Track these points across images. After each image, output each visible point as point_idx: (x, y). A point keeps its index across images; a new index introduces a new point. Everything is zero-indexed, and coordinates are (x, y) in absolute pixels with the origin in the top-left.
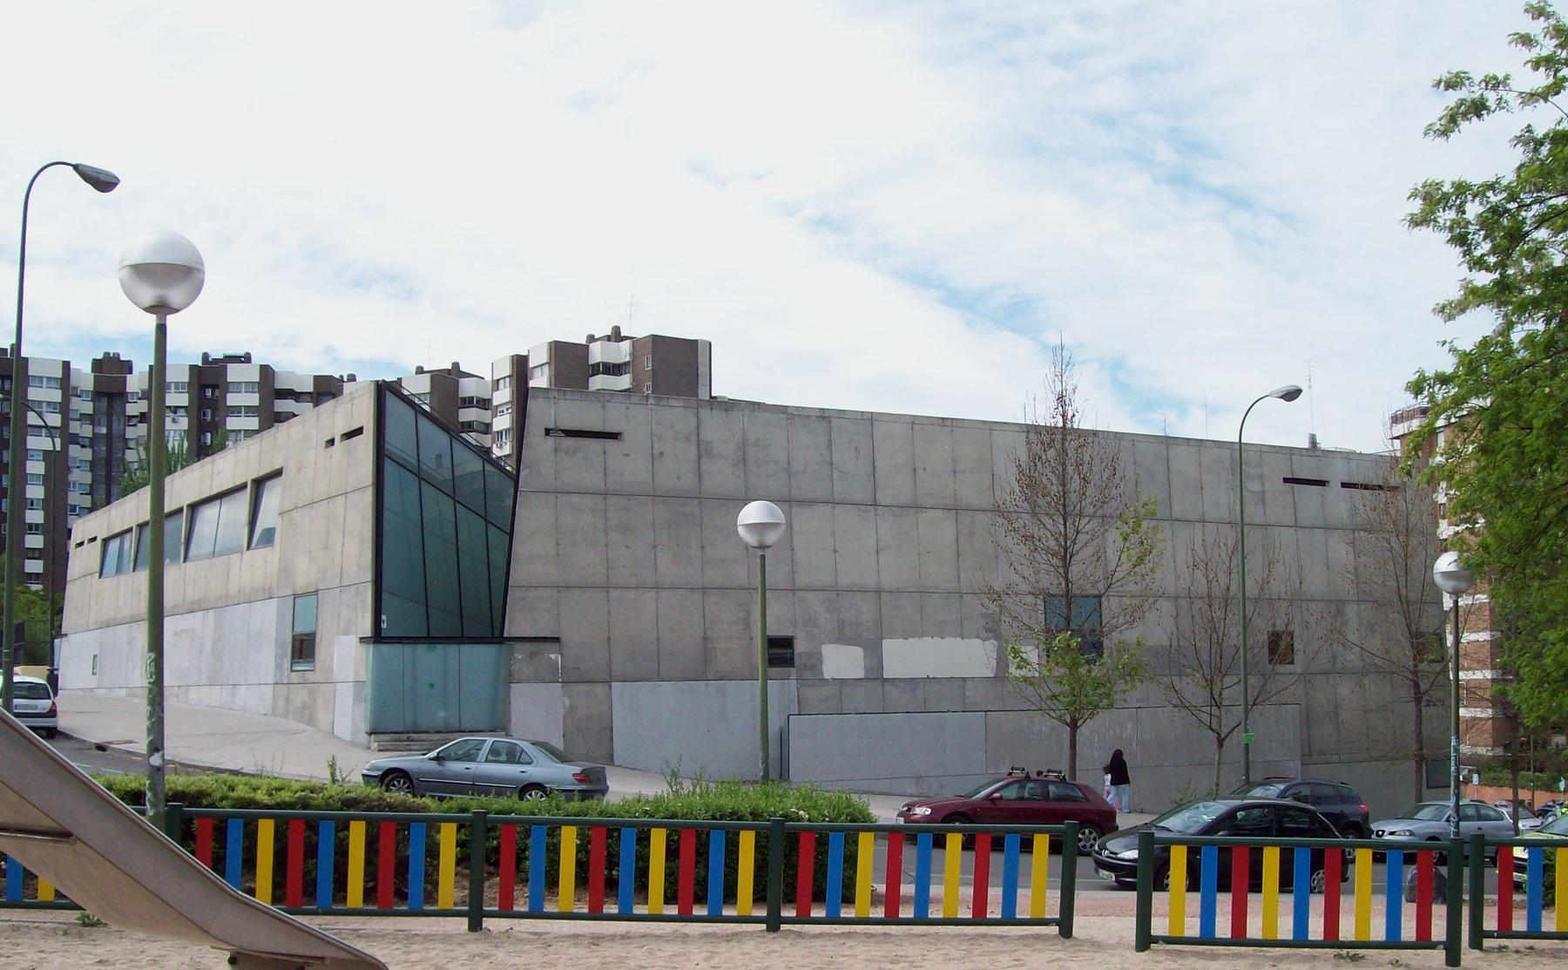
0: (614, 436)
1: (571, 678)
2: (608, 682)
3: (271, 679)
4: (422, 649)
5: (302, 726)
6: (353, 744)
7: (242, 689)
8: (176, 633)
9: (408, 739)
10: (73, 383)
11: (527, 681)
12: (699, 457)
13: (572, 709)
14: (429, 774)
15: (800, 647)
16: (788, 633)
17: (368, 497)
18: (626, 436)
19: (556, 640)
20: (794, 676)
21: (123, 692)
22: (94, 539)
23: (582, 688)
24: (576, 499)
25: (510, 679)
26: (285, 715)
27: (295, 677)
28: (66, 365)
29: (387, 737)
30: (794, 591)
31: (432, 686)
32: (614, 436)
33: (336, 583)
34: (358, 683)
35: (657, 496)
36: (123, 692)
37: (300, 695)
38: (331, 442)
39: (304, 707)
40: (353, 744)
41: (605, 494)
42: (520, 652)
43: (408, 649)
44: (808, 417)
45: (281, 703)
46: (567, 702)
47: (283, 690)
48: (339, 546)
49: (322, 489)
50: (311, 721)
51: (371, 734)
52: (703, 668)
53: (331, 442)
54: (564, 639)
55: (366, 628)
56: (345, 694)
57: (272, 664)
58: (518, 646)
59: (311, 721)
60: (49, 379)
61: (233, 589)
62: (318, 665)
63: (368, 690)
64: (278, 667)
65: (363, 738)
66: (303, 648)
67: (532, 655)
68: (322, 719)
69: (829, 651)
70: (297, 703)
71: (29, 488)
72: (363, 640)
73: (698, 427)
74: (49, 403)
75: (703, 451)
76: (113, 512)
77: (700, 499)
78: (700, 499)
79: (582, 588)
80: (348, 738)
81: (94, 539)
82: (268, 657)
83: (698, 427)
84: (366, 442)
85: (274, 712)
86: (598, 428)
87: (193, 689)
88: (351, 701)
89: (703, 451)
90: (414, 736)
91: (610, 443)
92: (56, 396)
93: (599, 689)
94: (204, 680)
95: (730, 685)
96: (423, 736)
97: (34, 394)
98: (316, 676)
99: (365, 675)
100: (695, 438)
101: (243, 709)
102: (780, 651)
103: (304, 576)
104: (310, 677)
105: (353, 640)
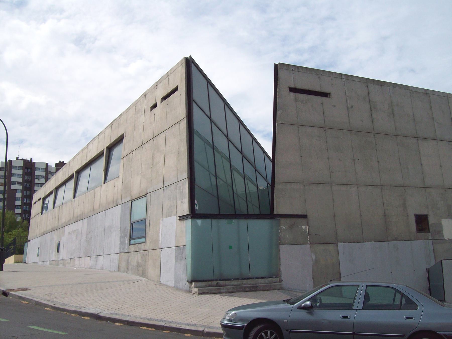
0: (326, 95)
1: (315, 241)
2: (336, 243)
3: (117, 250)
4: (223, 222)
5: (139, 278)
6: (177, 288)
7: (101, 258)
8: (69, 233)
9: (218, 285)
10: (49, 170)
11: (289, 244)
12: (371, 110)
13: (317, 261)
14: (300, 323)
15: (431, 220)
16: (425, 212)
17: (184, 125)
18: (333, 95)
19: (304, 216)
20: (430, 238)
21: (48, 263)
22: (40, 199)
23: (321, 247)
24: (309, 130)
25: (279, 242)
26: (127, 270)
27: (132, 248)
28: (47, 164)
29: (203, 284)
30: (425, 188)
31: (231, 247)
32: (326, 95)
33: (161, 185)
34: (180, 248)
35: (353, 131)
36: (48, 263)
37: (136, 258)
38: (155, 106)
39: (139, 265)
40: (177, 288)
41: (325, 128)
42: (284, 224)
43: (214, 222)
44: (419, 93)
45: (124, 264)
46: (314, 257)
47: (125, 256)
48: (161, 164)
49: (149, 134)
50: (144, 274)
51: (191, 282)
52: (385, 235)
53: (155, 106)
54: (309, 216)
55: (185, 208)
56: (168, 258)
57: (118, 242)
58: (283, 220)
59: (144, 274)
60: (42, 168)
61: (97, 206)
62: (148, 240)
63: (188, 251)
64: (122, 243)
65: (185, 284)
66: (136, 231)
67: (291, 227)
68: (152, 272)
69: (445, 223)
70: (134, 263)
71: (21, 188)
72: (182, 218)
73: (369, 94)
74: (41, 176)
75: (372, 107)
76: (47, 186)
77: (374, 134)
78: (374, 134)
79: (318, 184)
80: (172, 284)
81: (40, 199)
82: (115, 241)
83: (369, 94)
84: (180, 99)
85: (119, 269)
86: (318, 89)
87: (76, 259)
88: (174, 260)
89: (372, 107)
90: (221, 283)
91: (324, 99)
92: (44, 174)
93: (331, 247)
94: (82, 255)
95: (399, 243)
96: (227, 282)
97: (37, 173)
98: (147, 246)
99: (186, 239)
100: (367, 99)
101: (102, 268)
102: (422, 222)
103: (138, 185)
104: (142, 246)
105: (174, 219)
